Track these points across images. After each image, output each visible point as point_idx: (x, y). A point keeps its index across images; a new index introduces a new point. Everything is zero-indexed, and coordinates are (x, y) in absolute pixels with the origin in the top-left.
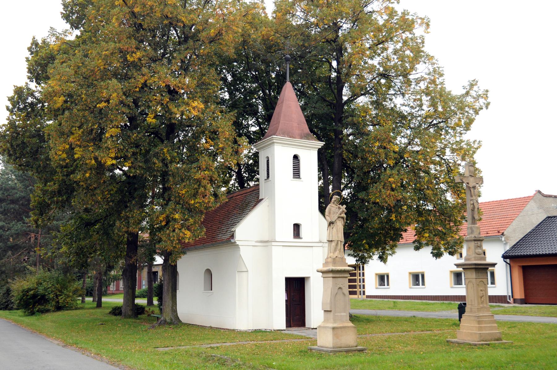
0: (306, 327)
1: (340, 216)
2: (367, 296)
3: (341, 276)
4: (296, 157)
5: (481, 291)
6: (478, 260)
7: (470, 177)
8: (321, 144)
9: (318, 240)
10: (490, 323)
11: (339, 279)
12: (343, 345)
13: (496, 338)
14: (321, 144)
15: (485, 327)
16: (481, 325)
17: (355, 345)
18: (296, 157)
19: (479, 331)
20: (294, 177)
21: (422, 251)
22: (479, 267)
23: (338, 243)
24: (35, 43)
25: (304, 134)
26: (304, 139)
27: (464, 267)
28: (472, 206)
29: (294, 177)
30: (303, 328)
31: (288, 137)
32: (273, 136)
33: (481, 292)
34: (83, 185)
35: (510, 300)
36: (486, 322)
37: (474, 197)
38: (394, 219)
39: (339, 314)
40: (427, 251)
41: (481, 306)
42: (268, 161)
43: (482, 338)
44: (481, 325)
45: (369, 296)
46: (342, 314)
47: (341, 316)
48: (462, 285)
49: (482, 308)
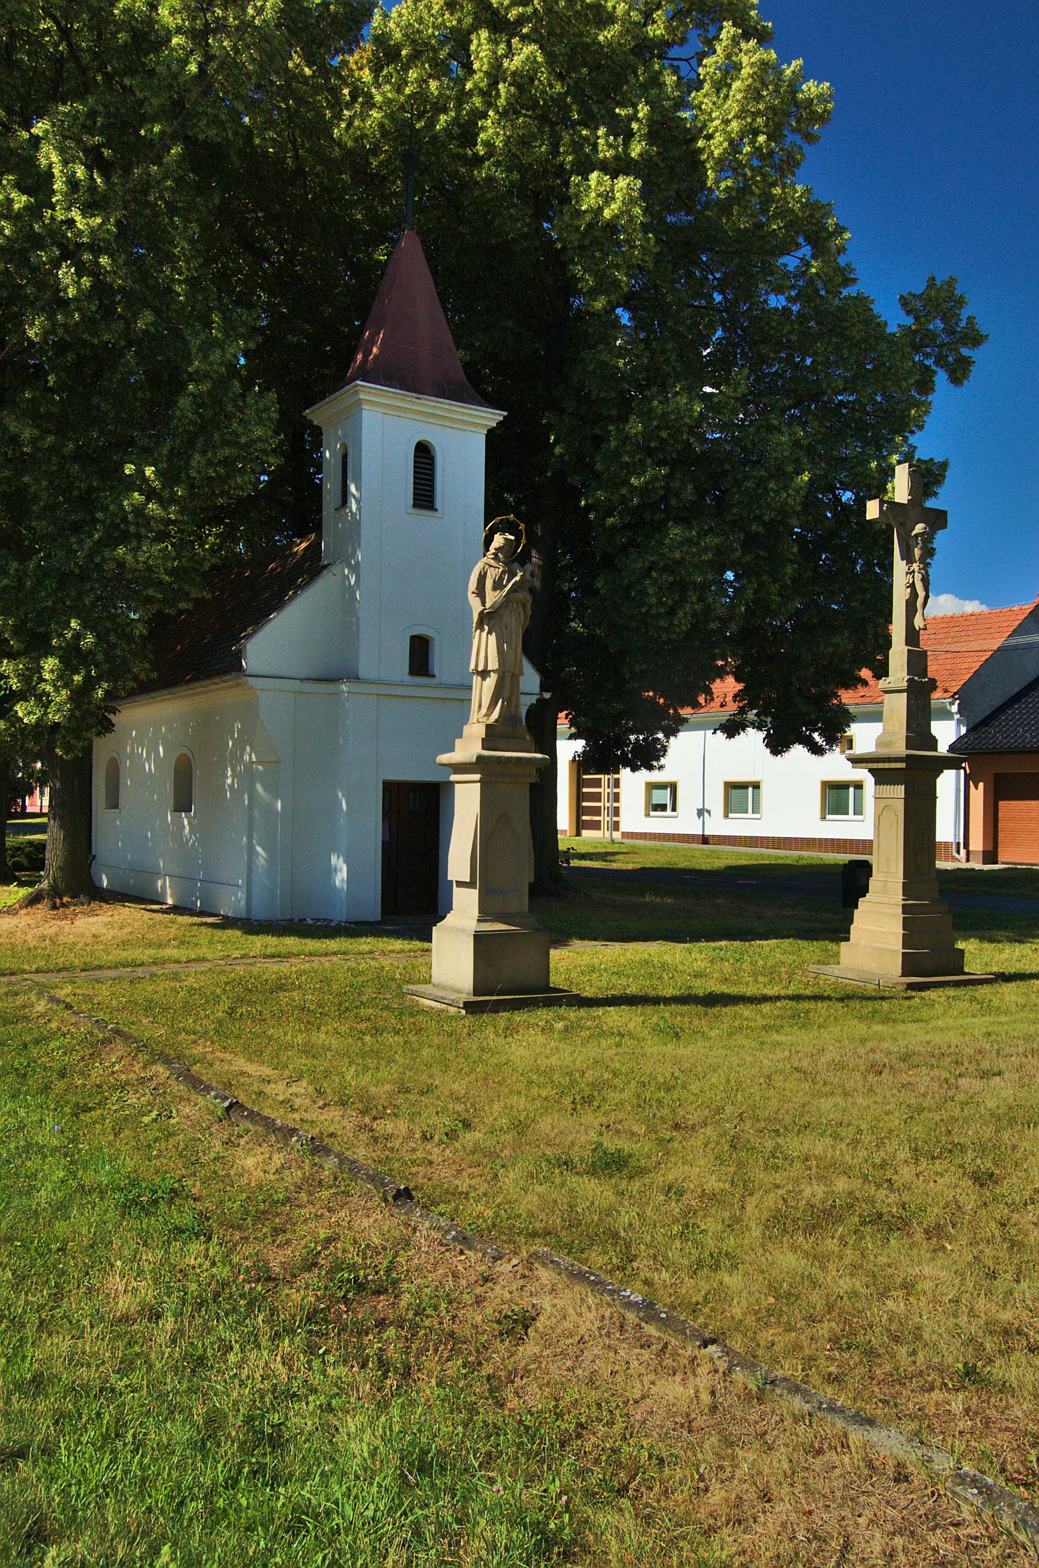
2: (623, 833)
4: (424, 453)
8: (493, 417)
14: (493, 417)
18: (424, 453)
21: (741, 738)
24: (848, 939)
27: (875, 766)
28: (909, 590)
29: (415, 506)
31: (401, 389)
32: (358, 382)
35: (958, 852)
40: (753, 739)
42: (345, 457)
45: (628, 833)
48: (847, 813)
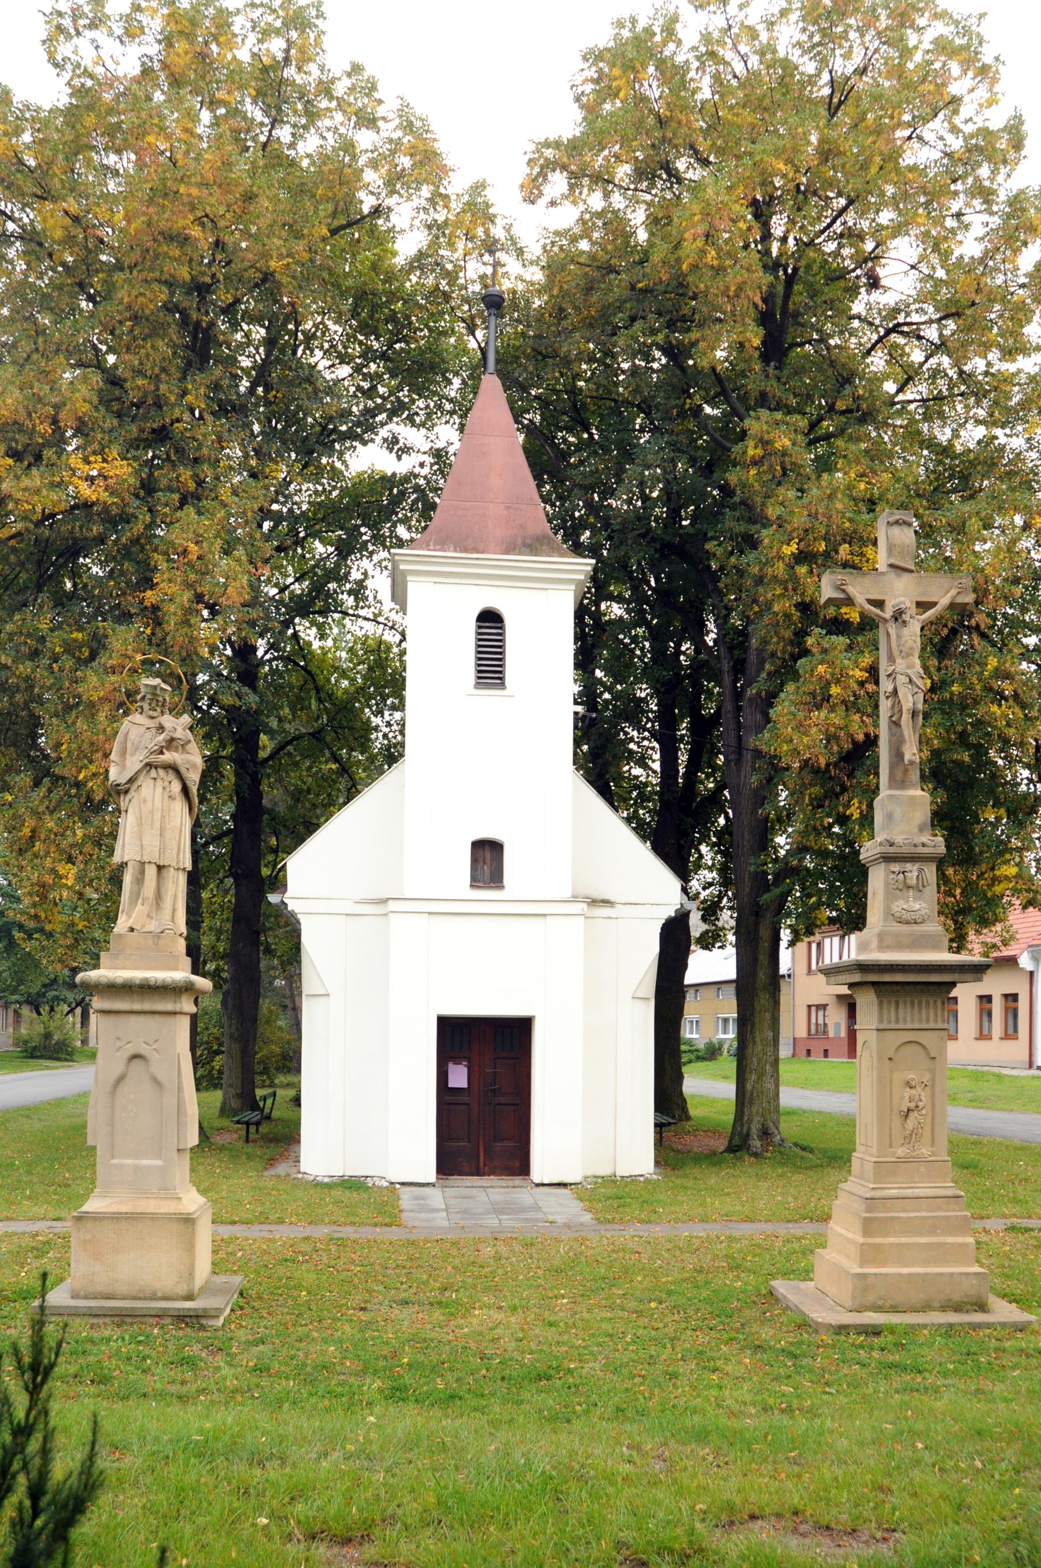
0: (538, 1172)
1: (153, 758)
3: (137, 1007)
4: (490, 619)
5: (909, 1085)
6: (900, 947)
7: (892, 575)
9: (567, 894)
10: (932, 1230)
11: (133, 1019)
12: (122, 1289)
13: (957, 1297)
15: (901, 1245)
16: (878, 1240)
17: (182, 1289)
18: (490, 619)
19: (863, 1263)
20: (478, 685)
22: (887, 978)
23: (142, 872)
25: (524, 538)
26: (520, 554)
29: (478, 685)
30: (517, 1181)
31: (455, 551)
33: (908, 1092)
34: (318, 795)
36: (908, 1227)
37: (899, 661)
38: (856, 816)
39: (129, 1161)
41: (901, 1152)
43: (871, 1298)
44: (878, 1240)
46: (145, 1162)
47: (137, 1168)
49: (901, 1161)
